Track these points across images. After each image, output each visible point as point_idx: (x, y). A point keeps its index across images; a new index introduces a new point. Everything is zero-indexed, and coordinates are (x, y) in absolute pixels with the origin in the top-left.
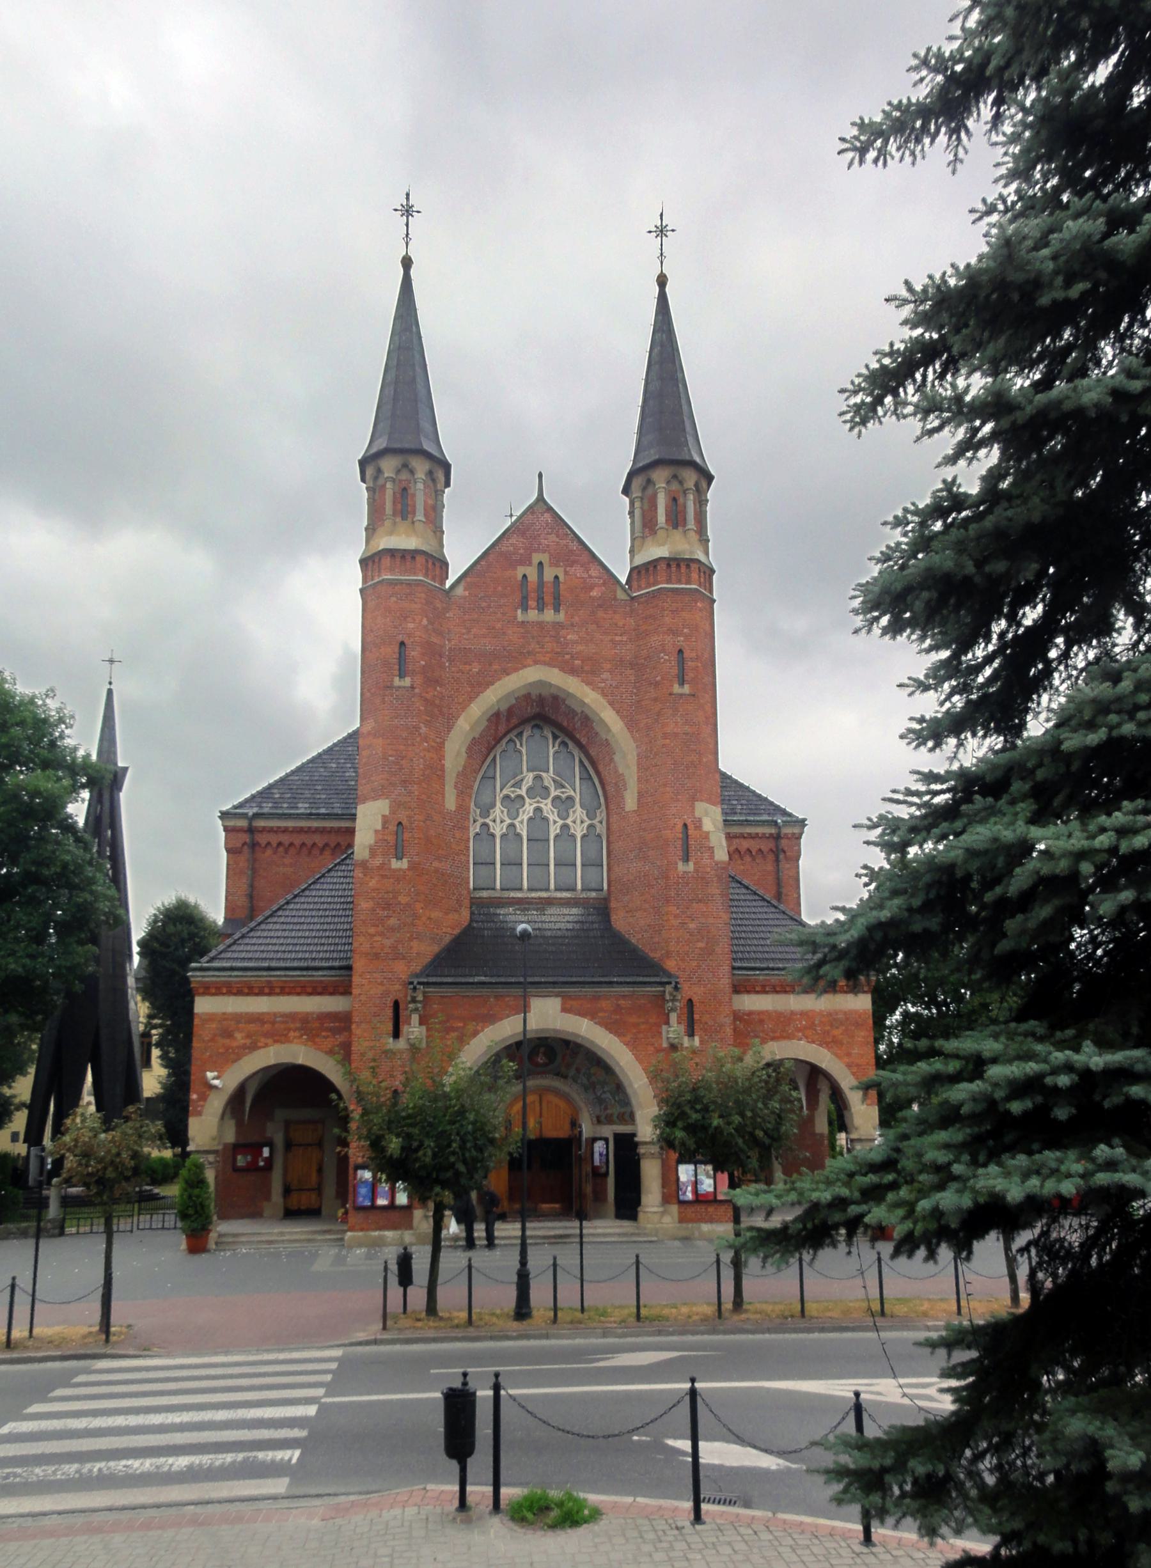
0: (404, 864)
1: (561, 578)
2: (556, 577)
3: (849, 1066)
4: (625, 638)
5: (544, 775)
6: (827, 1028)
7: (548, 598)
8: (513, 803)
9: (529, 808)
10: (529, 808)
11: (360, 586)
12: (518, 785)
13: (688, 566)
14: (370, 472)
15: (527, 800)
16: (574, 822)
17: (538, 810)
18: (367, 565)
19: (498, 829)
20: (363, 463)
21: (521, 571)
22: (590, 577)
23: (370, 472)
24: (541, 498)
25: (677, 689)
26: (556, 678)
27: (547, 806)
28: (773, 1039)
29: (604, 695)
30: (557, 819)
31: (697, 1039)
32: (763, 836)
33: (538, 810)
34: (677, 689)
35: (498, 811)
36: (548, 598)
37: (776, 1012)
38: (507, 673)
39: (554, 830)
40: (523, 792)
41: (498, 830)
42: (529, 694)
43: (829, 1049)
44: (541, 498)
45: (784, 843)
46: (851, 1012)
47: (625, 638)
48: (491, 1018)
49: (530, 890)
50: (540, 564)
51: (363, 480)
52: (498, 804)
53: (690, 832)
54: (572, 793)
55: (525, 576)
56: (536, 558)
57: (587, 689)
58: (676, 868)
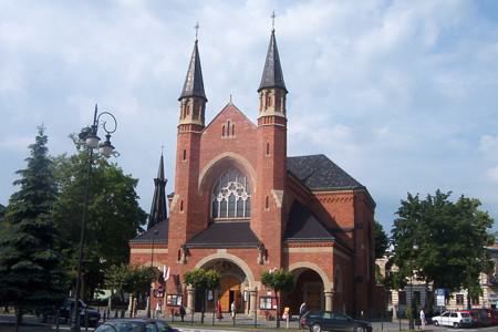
7: (231, 131)
10: (230, 192)
26: (232, 155)
27: (235, 192)
36: (231, 131)
48: (206, 255)
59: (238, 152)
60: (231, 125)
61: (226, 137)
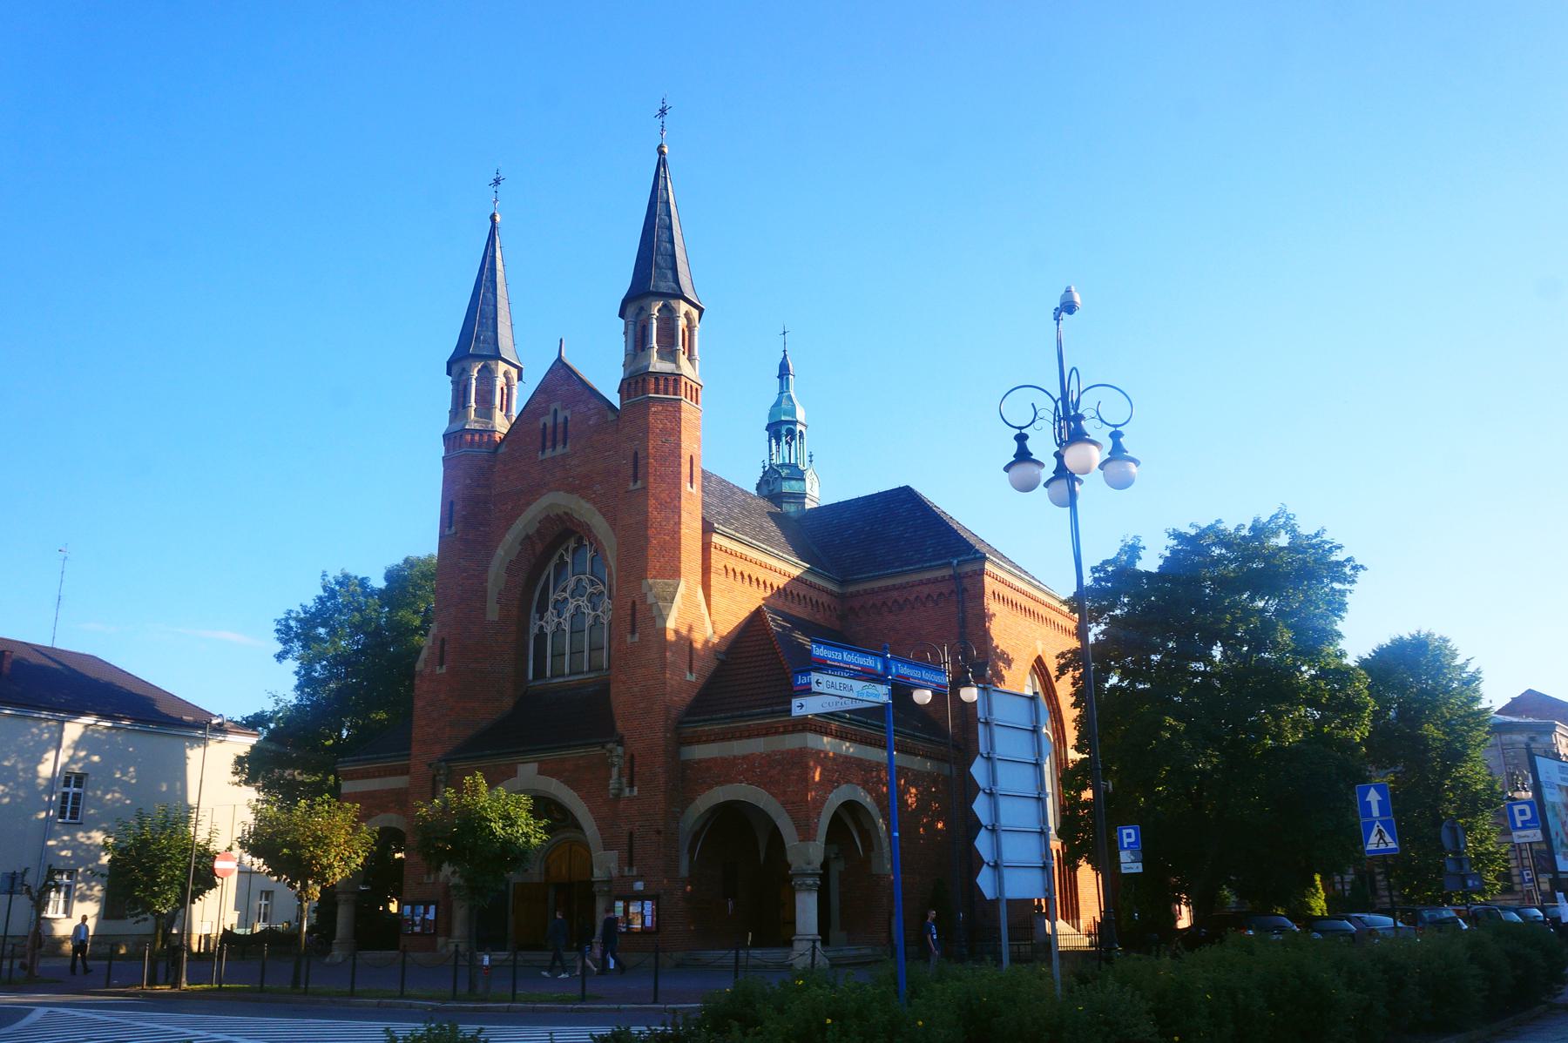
0: (444, 670)
1: (569, 419)
2: (566, 418)
3: (784, 804)
4: (611, 453)
5: (582, 576)
6: (766, 769)
7: (560, 436)
8: (560, 605)
9: (571, 605)
10: (571, 605)
11: (443, 455)
12: (564, 590)
13: (644, 380)
14: (455, 369)
15: (570, 600)
16: (604, 613)
17: (578, 607)
18: (449, 439)
19: (549, 628)
20: (450, 364)
21: (542, 420)
22: (589, 409)
23: (455, 369)
24: (560, 358)
25: (631, 487)
26: (554, 500)
27: (583, 602)
28: (717, 784)
29: (595, 503)
30: (590, 612)
31: (636, 789)
32: (943, 579)
33: (578, 607)
34: (631, 487)
35: (550, 613)
36: (560, 436)
37: (721, 758)
38: (528, 504)
39: (588, 622)
40: (567, 595)
41: (549, 630)
42: (548, 516)
43: (765, 788)
44: (560, 358)
45: (967, 583)
46: (788, 752)
47: (611, 453)
49: (571, 674)
50: (556, 410)
51: (449, 373)
52: (550, 608)
53: (638, 607)
54: (602, 588)
55: (545, 424)
56: (552, 407)
57: (583, 502)
58: (625, 641)
59: (572, 489)
60: (560, 419)
61: (549, 453)
